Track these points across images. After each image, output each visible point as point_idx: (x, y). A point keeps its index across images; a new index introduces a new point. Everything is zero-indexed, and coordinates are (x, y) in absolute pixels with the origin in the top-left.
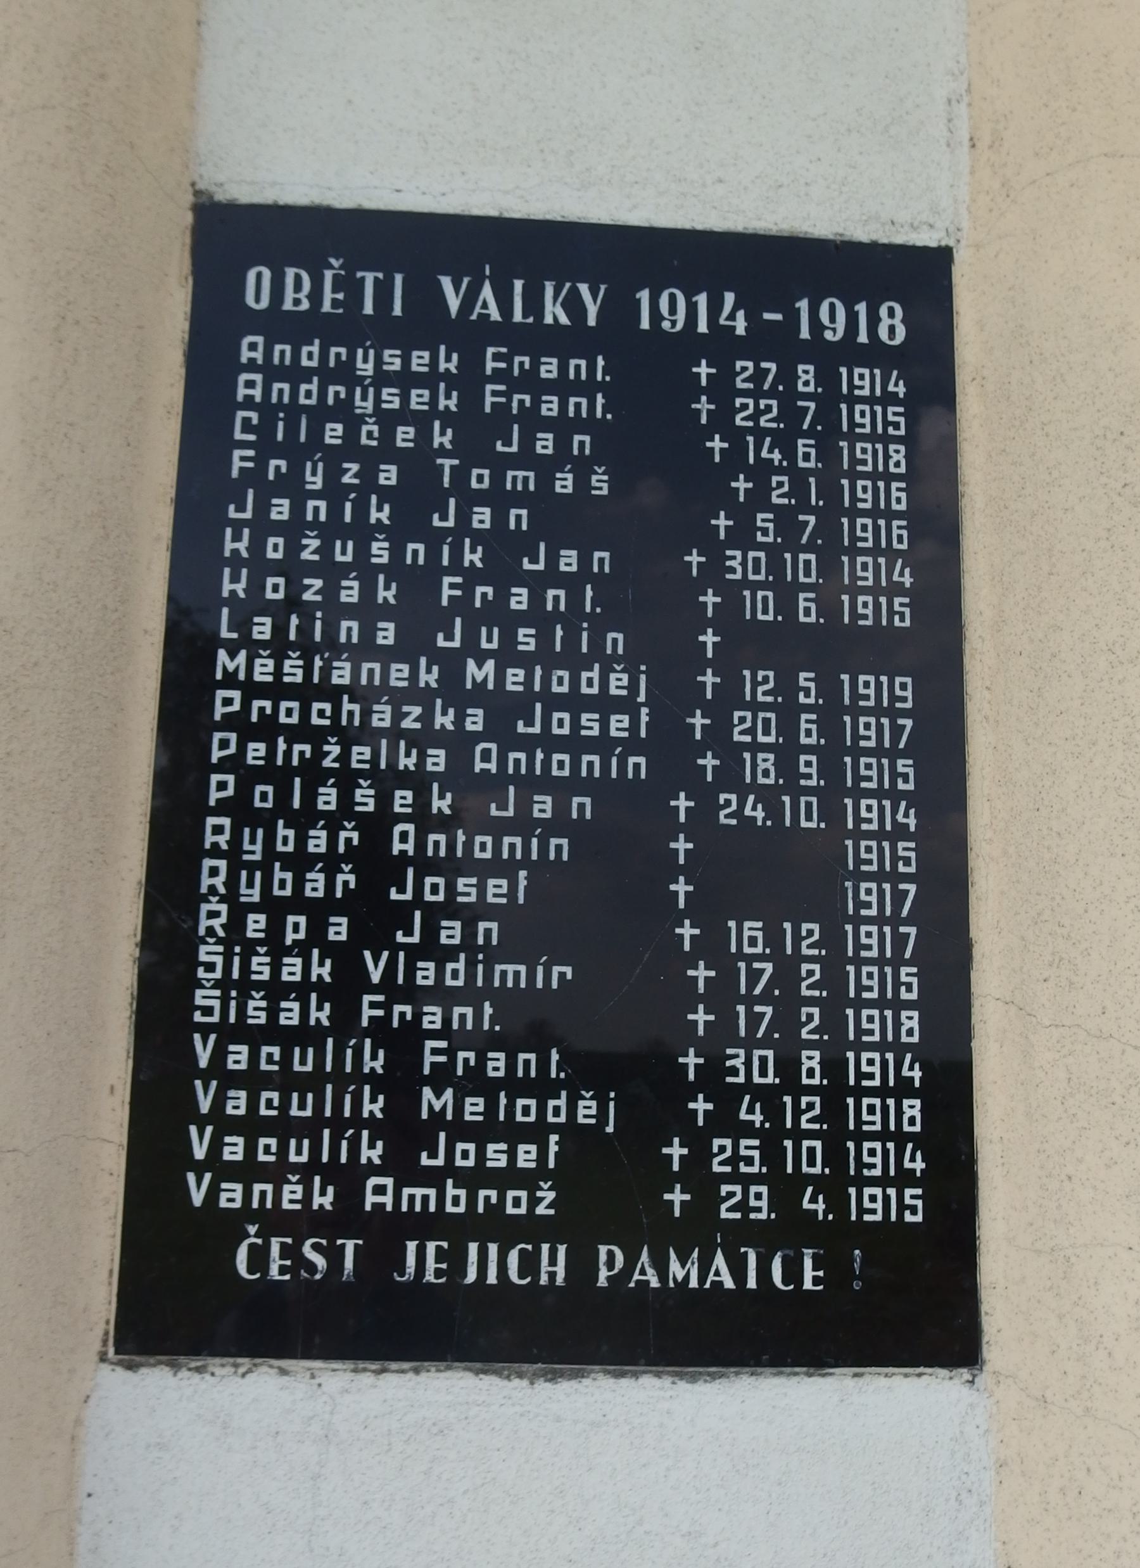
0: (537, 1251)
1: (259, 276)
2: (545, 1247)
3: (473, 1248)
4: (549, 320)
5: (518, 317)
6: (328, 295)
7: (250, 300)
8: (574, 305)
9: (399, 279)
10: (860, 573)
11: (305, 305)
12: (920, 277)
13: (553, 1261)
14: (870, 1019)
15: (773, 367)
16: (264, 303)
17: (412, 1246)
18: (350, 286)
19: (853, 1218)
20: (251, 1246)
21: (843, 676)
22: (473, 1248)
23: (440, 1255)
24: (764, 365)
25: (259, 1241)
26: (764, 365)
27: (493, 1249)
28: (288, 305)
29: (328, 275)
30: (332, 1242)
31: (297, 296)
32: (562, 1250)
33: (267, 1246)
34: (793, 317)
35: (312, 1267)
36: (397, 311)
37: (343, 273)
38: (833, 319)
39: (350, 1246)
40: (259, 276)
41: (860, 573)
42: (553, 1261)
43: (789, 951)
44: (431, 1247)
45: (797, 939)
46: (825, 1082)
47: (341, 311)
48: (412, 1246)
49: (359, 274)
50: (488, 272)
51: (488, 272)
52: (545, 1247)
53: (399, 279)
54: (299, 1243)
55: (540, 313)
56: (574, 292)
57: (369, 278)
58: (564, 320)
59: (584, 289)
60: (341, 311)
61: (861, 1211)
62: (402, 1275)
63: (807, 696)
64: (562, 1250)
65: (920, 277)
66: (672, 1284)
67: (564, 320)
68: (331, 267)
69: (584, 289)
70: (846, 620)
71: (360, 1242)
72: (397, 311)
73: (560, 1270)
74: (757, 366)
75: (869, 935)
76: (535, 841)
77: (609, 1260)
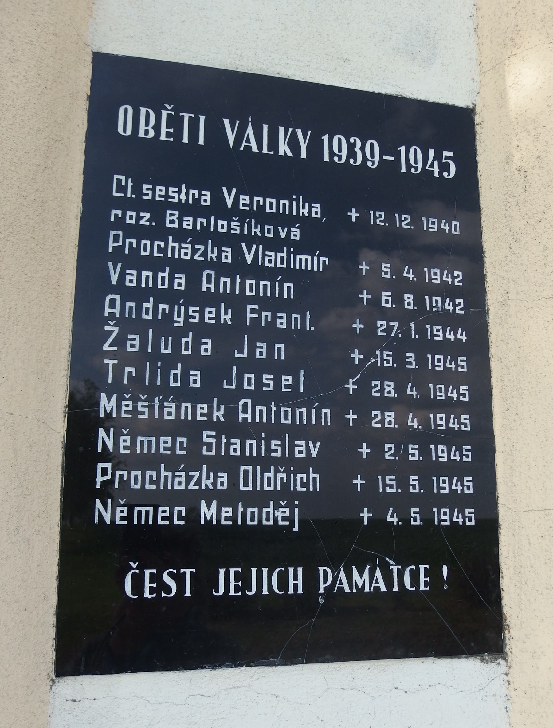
0: (287, 571)
1: (126, 110)
2: (291, 570)
3: (254, 571)
4: (281, 153)
5: (265, 150)
6: (164, 130)
7: (120, 130)
8: (294, 144)
9: (202, 118)
10: (437, 364)
11: (152, 134)
12: (453, 127)
13: (295, 578)
14: (436, 274)
15: (396, 324)
16: (129, 132)
17: (222, 572)
18: (175, 122)
19: (435, 491)
20: (134, 574)
21: (423, 218)
22: (254, 571)
23: (238, 577)
24: (391, 323)
25: (137, 571)
26: (391, 323)
27: (265, 571)
28: (142, 134)
29: (164, 113)
30: (178, 571)
31: (147, 128)
32: (300, 570)
33: (142, 574)
34: (398, 156)
35: (168, 590)
36: (201, 142)
37: (173, 113)
38: (416, 162)
39: (188, 572)
40: (126, 110)
41: (437, 364)
42: (295, 578)
43: (398, 225)
44: (232, 571)
45: (401, 221)
46: (416, 308)
47: (171, 139)
48: (222, 572)
49: (181, 114)
50: (250, 120)
51: (250, 120)
52: (291, 570)
53: (202, 118)
54: (160, 574)
55: (277, 150)
56: (294, 134)
57: (186, 117)
58: (290, 154)
59: (299, 132)
60: (171, 139)
61: (436, 425)
62: (217, 591)
63: (414, 488)
64: (300, 570)
65: (453, 127)
66: (355, 591)
67: (290, 154)
68: (166, 109)
69: (299, 132)
70: (427, 280)
71: (194, 570)
72: (201, 142)
73: (300, 582)
74: (387, 324)
75: (433, 223)
76: (277, 284)
77: (325, 577)
